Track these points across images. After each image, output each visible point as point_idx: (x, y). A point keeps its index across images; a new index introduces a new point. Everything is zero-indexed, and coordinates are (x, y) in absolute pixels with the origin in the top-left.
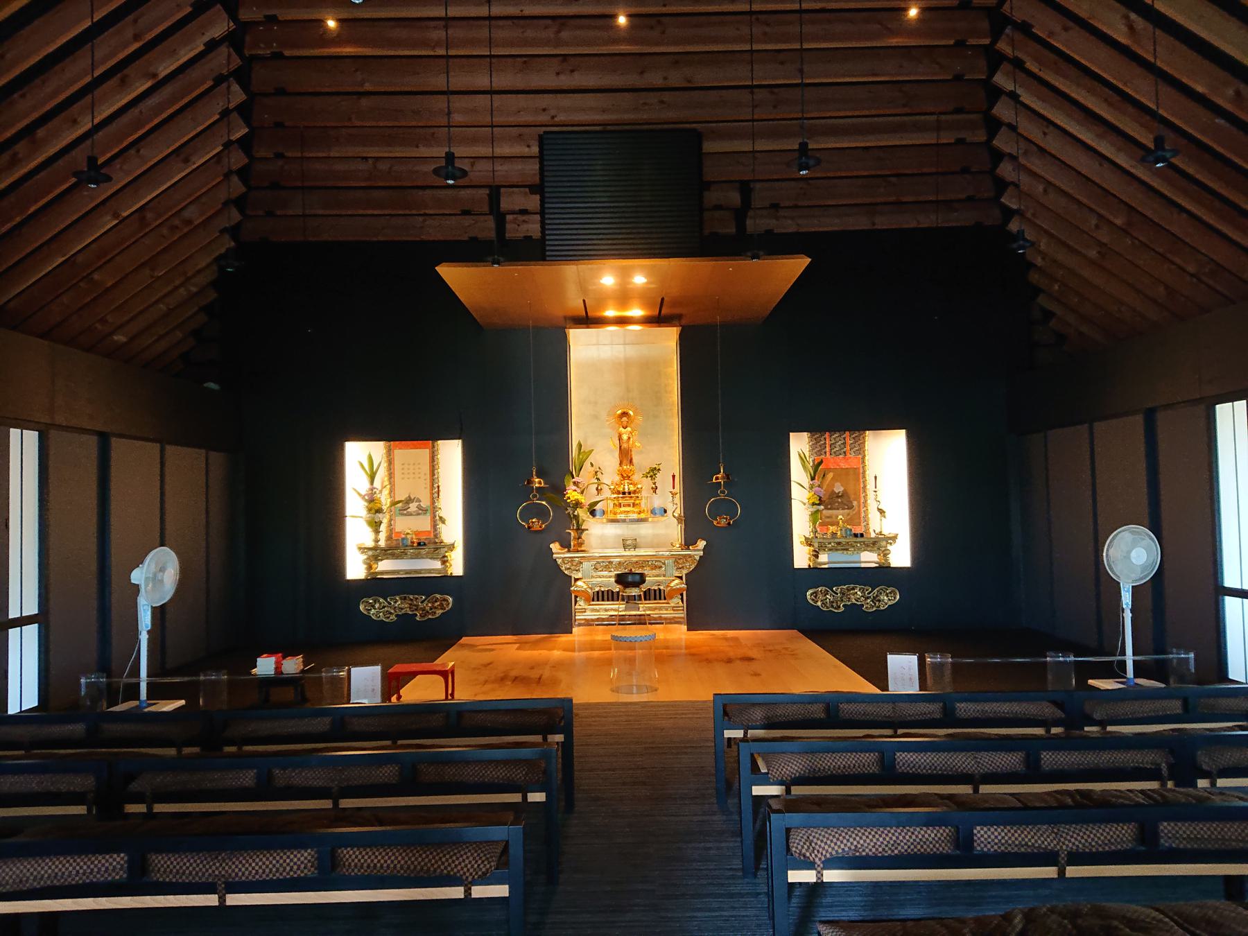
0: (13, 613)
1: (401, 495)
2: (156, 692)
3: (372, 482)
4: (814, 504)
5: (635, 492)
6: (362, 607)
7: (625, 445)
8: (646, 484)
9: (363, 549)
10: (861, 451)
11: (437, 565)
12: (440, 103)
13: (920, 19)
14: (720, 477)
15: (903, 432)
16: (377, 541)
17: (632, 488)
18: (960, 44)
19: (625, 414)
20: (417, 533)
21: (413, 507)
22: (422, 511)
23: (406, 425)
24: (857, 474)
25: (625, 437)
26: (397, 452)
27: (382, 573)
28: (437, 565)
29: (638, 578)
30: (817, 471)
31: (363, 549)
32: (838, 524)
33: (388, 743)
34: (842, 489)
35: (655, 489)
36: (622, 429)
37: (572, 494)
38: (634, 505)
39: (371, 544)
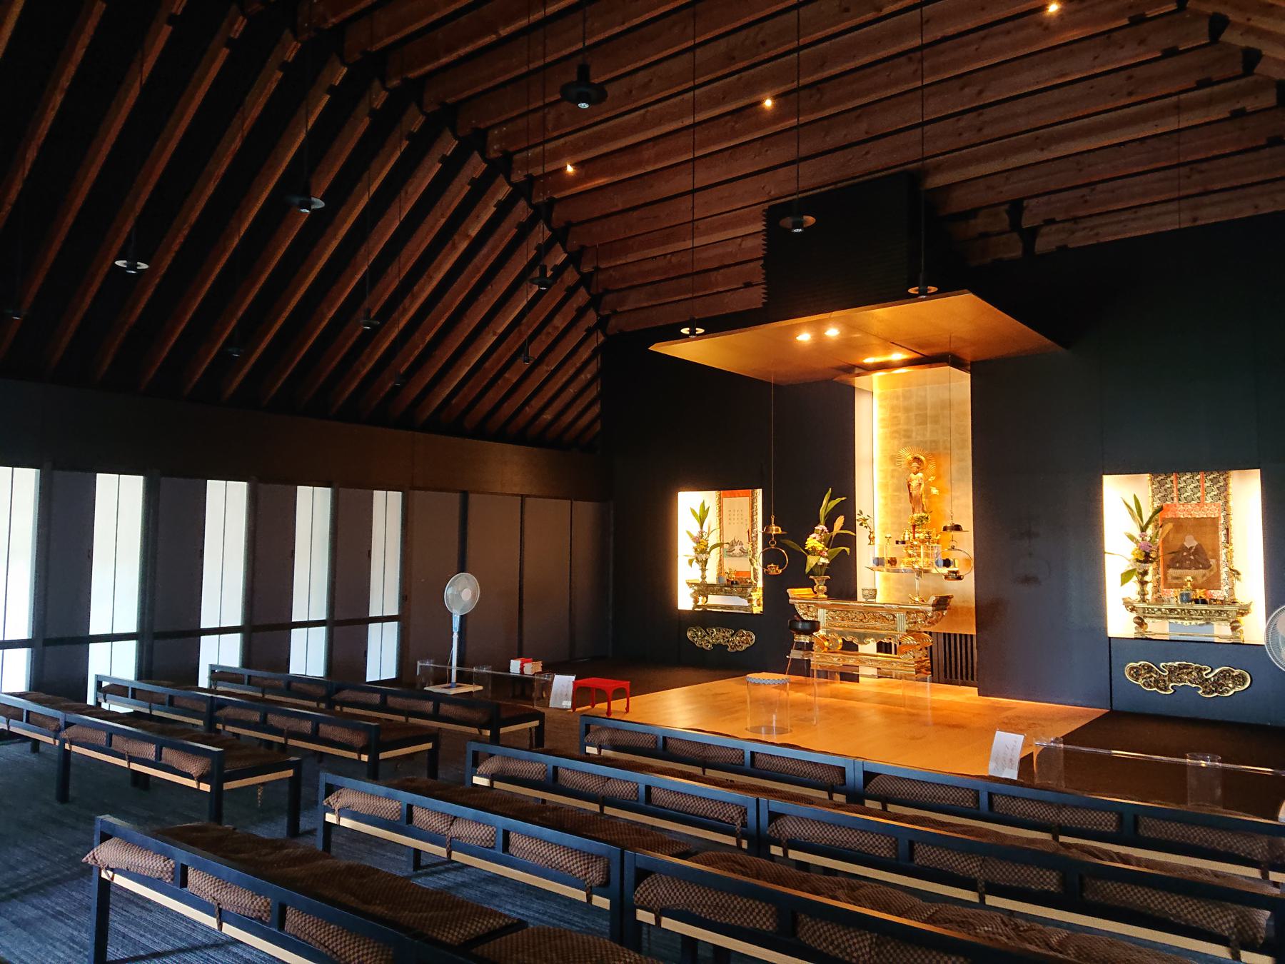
0: (374, 612)
1: (728, 539)
2: (463, 678)
4: (1138, 560)
6: (689, 634)
7: (914, 493)
9: (690, 584)
11: (744, 603)
12: (686, 203)
13: (775, 106)
15: (1256, 473)
16: (704, 578)
18: (1138, 20)
20: (737, 573)
21: (737, 548)
22: (744, 553)
23: (724, 479)
25: (914, 484)
26: (725, 500)
27: (715, 607)
28: (744, 603)
29: (807, 626)
31: (690, 584)
33: (314, 704)
34: (1195, 543)
39: (699, 581)
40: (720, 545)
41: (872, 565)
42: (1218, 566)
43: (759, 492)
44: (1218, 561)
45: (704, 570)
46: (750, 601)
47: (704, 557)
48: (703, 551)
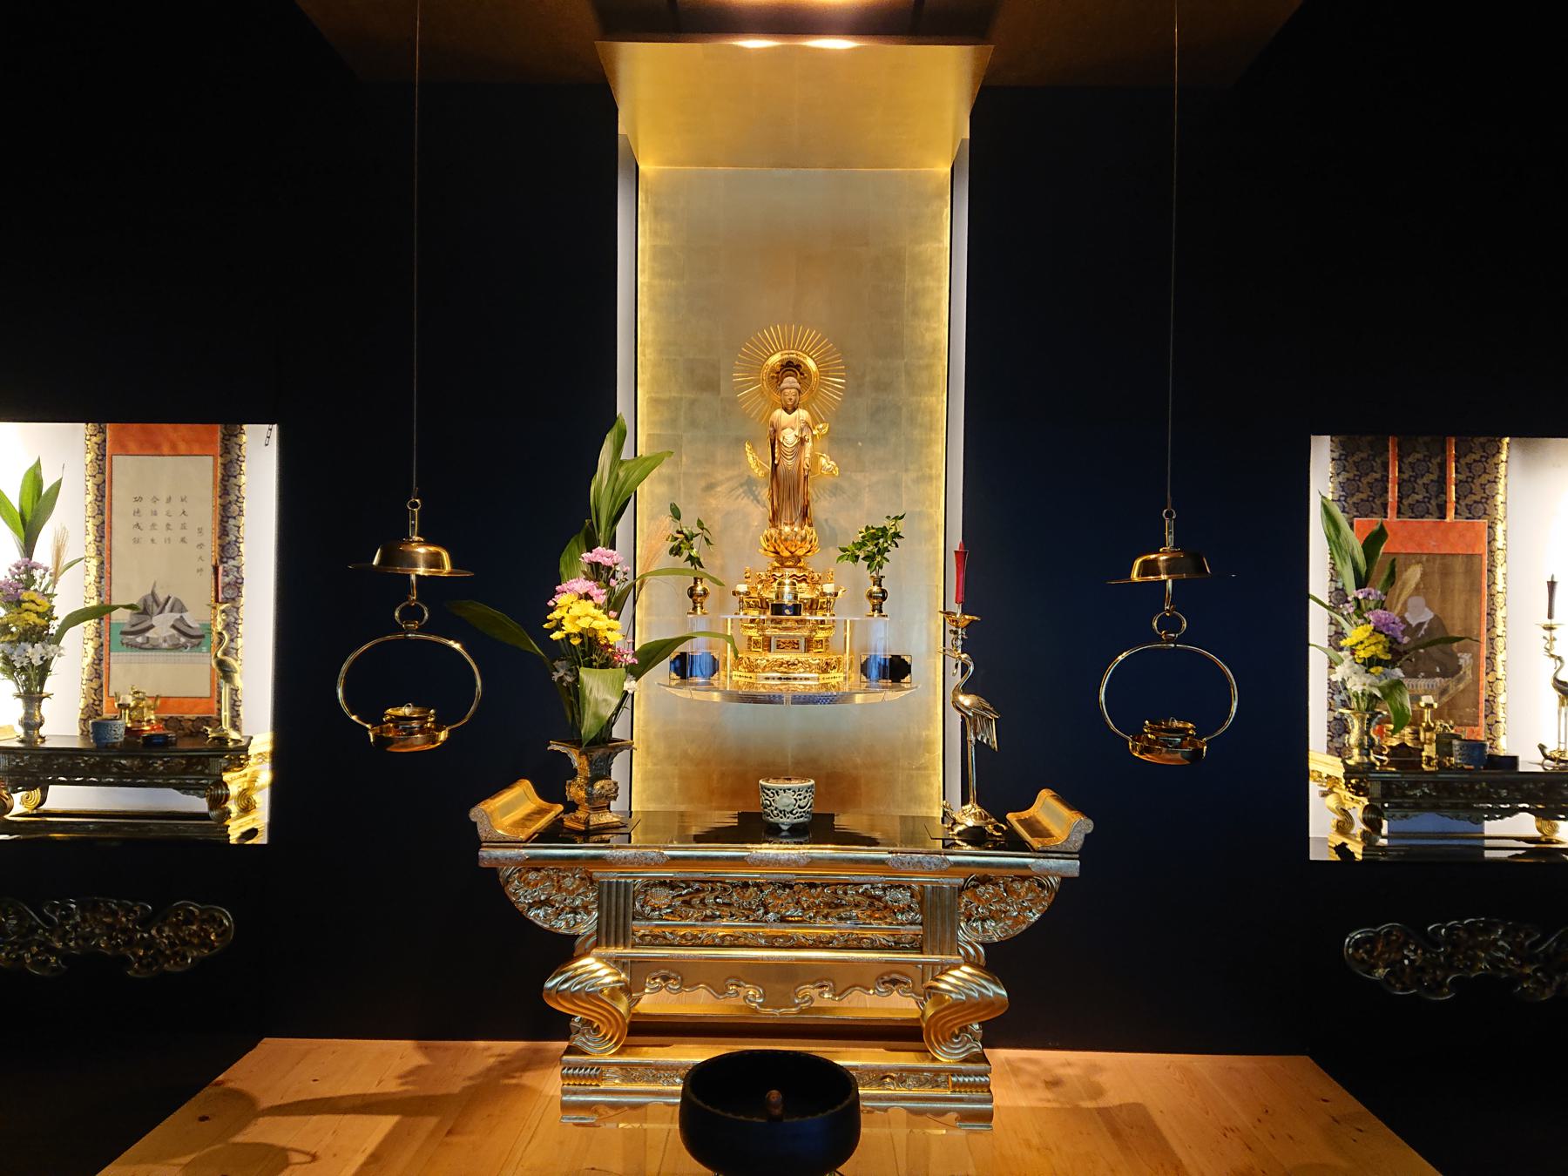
1: (128, 591)
3: (28, 546)
5: (813, 606)
7: (788, 463)
8: (843, 581)
10: (1478, 503)
11: (199, 804)
14: (1157, 565)
16: (31, 724)
17: (805, 592)
19: (791, 367)
20: (161, 702)
21: (162, 626)
24: (1469, 575)
25: (789, 437)
26: (125, 467)
30: (1374, 568)
32: (1416, 721)
34: (1427, 616)
35: (879, 600)
36: (779, 414)
37: (575, 610)
38: (809, 644)
40: (100, 612)
41: (901, 526)
42: (1476, 668)
43: (260, 450)
44: (1476, 657)
45: (32, 697)
46: (1412, 558)
47: (35, 653)
48: (35, 634)
